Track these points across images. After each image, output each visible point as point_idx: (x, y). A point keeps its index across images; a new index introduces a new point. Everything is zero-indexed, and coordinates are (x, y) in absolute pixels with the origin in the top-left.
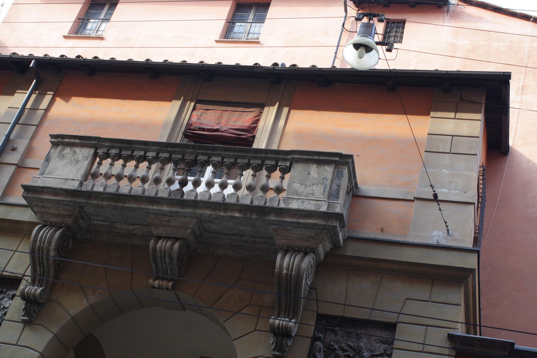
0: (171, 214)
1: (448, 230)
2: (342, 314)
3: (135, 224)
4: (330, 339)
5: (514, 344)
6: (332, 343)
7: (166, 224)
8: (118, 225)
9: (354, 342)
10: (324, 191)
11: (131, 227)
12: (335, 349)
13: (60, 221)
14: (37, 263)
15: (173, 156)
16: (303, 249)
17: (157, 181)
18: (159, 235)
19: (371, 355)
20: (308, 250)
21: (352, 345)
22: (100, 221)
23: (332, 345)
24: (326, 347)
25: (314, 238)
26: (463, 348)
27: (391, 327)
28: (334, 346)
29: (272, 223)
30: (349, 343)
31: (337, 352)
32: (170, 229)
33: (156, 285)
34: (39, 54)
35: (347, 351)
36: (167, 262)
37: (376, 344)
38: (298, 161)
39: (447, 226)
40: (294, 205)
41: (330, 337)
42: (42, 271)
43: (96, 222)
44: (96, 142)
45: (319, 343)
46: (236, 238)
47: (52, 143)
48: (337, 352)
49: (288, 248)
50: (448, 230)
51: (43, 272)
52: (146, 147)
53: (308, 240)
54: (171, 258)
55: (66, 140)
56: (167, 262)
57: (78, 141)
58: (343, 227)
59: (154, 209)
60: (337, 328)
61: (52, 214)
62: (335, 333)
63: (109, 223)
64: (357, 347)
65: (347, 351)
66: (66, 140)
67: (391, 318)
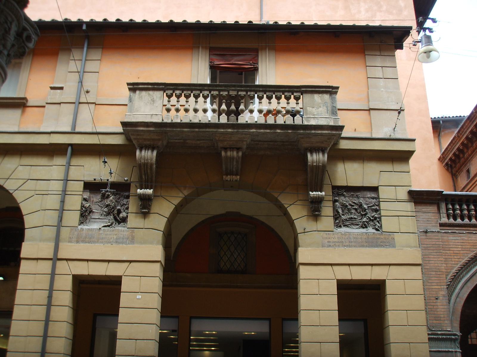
0: (232, 133)
1: (395, 128)
2: (346, 185)
3: (201, 140)
4: (342, 200)
5: (443, 191)
6: (344, 202)
7: (228, 139)
8: (188, 141)
9: (356, 200)
10: (328, 111)
11: (198, 142)
12: (347, 206)
13: (152, 143)
14: (143, 172)
15: (221, 93)
16: (320, 148)
17: (205, 111)
18: (224, 147)
19: (368, 207)
20: (324, 149)
21: (356, 202)
22: (176, 139)
23: (345, 204)
24: (341, 205)
25: (326, 141)
26: (417, 197)
27: (375, 189)
28: (346, 204)
29: (301, 134)
30: (353, 201)
31: (348, 207)
32: (232, 142)
33: (229, 179)
34: (86, 19)
35: (353, 206)
36: (235, 164)
37: (369, 200)
38: (306, 92)
39: (395, 126)
40: (313, 122)
41: (342, 199)
42: (146, 178)
43: (172, 141)
44: (164, 87)
45: (337, 203)
46: (271, 143)
47: (130, 89)
48: (348, 207)
49: (311, 148)
50: (395, 128)
51: (147, 178)
52: (200, 88)
53: (323, 143)
54: (237, 162)
55: (140, 86)
56: (235, 164)
57: (150, 86)
58: (131, 102)
59: (222, 131)
60: (344, 193)
61: (145, 139)
62: (344, 195)
63: (182, 141)
64: (359, 203)
65: (353, 206)
66: (140, 86)
67: (375, 185)
